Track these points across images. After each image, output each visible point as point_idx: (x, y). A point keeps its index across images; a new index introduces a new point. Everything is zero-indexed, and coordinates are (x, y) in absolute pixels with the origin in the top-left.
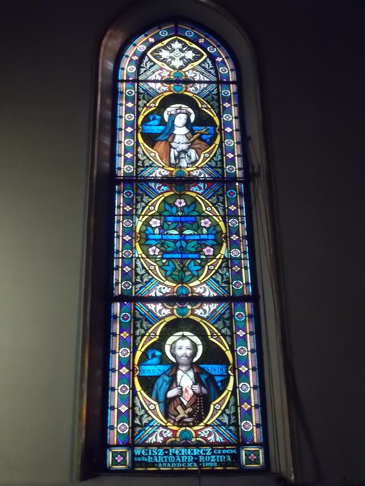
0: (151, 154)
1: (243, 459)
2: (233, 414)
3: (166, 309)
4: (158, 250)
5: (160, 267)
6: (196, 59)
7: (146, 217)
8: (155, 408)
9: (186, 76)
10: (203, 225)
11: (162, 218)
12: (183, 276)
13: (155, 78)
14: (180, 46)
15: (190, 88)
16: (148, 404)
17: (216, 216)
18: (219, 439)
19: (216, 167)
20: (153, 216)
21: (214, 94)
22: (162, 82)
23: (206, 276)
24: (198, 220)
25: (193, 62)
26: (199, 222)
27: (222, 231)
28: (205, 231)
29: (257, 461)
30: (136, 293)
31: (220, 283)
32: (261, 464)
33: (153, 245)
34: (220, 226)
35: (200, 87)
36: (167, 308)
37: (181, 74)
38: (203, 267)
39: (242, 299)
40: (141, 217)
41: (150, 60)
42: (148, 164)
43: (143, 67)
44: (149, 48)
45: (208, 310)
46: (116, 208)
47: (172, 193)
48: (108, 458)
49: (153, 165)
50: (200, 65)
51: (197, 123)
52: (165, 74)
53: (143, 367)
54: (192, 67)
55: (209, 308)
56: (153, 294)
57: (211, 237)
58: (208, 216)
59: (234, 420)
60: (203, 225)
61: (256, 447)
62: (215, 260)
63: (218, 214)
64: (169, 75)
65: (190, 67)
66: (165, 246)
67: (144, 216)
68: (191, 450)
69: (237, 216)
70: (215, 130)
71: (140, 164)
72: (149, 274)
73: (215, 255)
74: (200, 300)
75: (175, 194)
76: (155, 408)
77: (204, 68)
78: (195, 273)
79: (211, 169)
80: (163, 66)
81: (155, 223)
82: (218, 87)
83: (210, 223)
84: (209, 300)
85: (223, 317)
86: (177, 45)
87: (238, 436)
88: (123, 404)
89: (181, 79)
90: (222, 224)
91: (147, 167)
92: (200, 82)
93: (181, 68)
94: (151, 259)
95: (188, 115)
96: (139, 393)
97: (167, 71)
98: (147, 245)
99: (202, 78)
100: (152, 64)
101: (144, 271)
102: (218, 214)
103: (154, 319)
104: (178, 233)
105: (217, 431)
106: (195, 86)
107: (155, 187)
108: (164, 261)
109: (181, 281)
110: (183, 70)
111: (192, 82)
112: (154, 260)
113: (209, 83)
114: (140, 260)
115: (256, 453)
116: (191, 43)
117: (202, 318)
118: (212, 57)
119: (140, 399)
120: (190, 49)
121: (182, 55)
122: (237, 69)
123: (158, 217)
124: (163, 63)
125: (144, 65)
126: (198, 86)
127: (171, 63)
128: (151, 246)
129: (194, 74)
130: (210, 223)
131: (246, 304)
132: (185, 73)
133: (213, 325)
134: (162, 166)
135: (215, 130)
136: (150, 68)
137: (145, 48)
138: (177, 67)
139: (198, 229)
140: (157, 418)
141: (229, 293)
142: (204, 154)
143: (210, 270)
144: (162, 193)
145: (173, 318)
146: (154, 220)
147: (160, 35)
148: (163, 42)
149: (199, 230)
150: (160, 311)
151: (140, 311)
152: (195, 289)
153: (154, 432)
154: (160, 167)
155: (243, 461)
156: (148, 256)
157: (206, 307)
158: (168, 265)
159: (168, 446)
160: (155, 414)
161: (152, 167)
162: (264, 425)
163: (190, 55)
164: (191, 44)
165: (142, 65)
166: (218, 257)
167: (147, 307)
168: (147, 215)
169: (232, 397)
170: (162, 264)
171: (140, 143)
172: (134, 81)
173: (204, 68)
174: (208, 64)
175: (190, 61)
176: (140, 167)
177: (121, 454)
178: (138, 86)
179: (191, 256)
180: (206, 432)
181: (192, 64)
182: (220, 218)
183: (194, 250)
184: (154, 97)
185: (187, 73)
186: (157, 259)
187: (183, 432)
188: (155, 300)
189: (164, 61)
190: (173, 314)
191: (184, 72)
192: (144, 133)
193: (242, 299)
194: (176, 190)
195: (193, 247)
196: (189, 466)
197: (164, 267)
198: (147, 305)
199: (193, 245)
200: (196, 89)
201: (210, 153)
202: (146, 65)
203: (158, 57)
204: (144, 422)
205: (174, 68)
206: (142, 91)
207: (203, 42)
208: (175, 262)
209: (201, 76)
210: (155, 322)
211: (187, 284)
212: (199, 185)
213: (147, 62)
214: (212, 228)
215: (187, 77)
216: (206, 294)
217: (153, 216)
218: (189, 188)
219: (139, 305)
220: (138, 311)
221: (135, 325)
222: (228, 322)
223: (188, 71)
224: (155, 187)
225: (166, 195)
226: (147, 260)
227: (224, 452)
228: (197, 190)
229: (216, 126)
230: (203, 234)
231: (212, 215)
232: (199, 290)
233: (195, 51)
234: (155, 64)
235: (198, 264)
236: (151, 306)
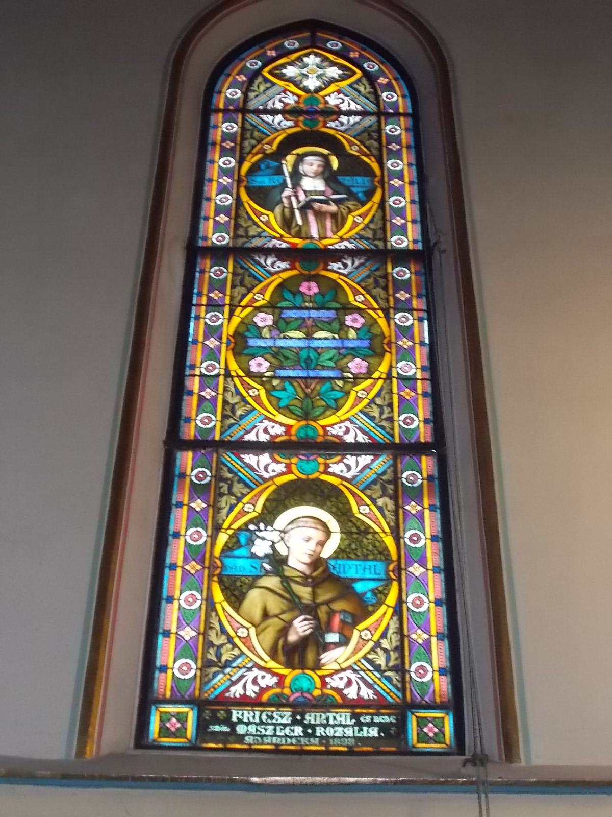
0: (261, 218)
1: (412, 734)
2: (396, 649)
3: (277, 464)
4: (267, 364)
5: (268, 392)
6: (342, 78)
7: (249, 310)
8: (249, 634)
9: (327, 102)
10: (348, 323)
11: (277, 311)
12: (310, 406)
13: (272, 106)
14: (318, 60)
15: (331, 122)
16: (234, 626)
17: (374, 309)
18: (367, 693)
19: (375, 239)
20: (259, 309)
21: (373, 131)
22: (283, 112)
23: (353, 407)
24: (341, 317)
25: (337, 81)
26: (342, 320)
27: (383, 334)
28: (352, 334)
29: (439, 737)
30: (222, 433)
31: (378, 420)
32: (448, 742)
33: (258, 355)
34: (380, 326)
35: (349, 121)
36: (278, 462)
37: (317, 100)
38: (348, 393)
39: (415, 449)
40: (239, 309)
41: (266, 80)
42: (255, 234)
43: (254, 91)
44: (264, 66)
45: (353, 465)
46: (195, 295)
47: (295, 272)
48: (427, 711)
49: (263, 234)
50: (351, 86)
51: (342, 170)
52: (291, 100)
53: (228, 561)
54: (337, 88)
55: (357, 462)
56: (251, 437)
57: (366, 343)
58: (358, 310)
59: (396, 659)
60: (348, 323)
61: (439, 711)
62: (369, 382)
63: (376, 306)
64: (297, 102)
65: (332, 88)
66: (280, 358)
67: (245, 307)
68: (267, 715)
69: (410, 310)
70: (373, 181)
71: (241, 232)
72: (235, 646)
73: (369, 374)
74: (339, 448)
75: (302, 274)
76: (249, 634)
77: (356, 90)
78: (332, 403)
79: (366, 242)
80: (287, 87)
81: (264, 320)
82: (379, 122)
83: (362, 320)
84: (357, 448)
85: (381, 479)
86: (312, 60)
87: (403, 690)
88: (188, 625)
89: (318, 109)
90: (382, 322)
91: (253, 237)
92: (349, 113)
93: (318, 90)
94: (253, 379)
95: (326, 158)
96: (218, 607)
97: (294, 94)
98: (247, 355)
99: (353, 106)
100: (268, 85)
101: (238, 397)
102: (376, 306)
103: (255, 482)
104: (305, 336)
105: (362, 679)
106: (340, 119)
107: (265, 262)
108: (276, 382)
109: (306, 416)
110: (322, 93)
111: (337, 113)
112: (257, 379)
113: (364, 114)
114: (233, 380)
115: (182, 718)
116: (336, 57)
117: (343, 478)
118: (370, 78)
119: (219, 617)
120: (333, 64)
121: (320, 71)
122: (413, 94)
123: (270, 310)
124: (287, 83)
125: (255, 87)
126: (344, 119)
127: (301, 83)
128: (253, 357)
129: (341, 101)
130: (362, 320)
131: (424, 458)
132: (324, 98)
133: (362, 491)
134: (278, 236)
135: (373, 181)
136: (264, 91)
137: (260, 63)
138: (312, 88)
139: (340, 330)
140: (253, 653)
141: (392, 436)
142: (354, 217)
143: (359, 400)
144: (277, 273)
145: (291, 477)
146: (261, 315)
147: (285, 47)
148: (289, 56)
149: (342, 333)
150: (266, 468)
151: (230, 465)
152: (329, 429)
153: (242, 676)
154: (275, 238)
155: (412, 739)
156: (249, 374)
157: (351, 460)
158: (284, 389)
159: (269, 704)
160: (247, 645)
161: (260, 237)
162: (454, 670)
163: (334, 72)
164: (335, 59)
165: (252, 88)
166: (376, 375)
167: (242, 460)
168: (251, 306)
169: (395, 618)
170: (272, 387)
171: (242, 202)
172: (237, 110)
173: (356, 90)
174: (364, 85)
175: (333, 81)
176: (242, 236)
177: (434, 722)
178: (244, 119)
179: (325, 374)
180: (341, 678)
181: (337, 84)
182: (380, 313)
183: (332, 364)
184: (262, 279)
185: (327, 98)
186: (264, 379)
187: (297, 679)
188: (257, 447)
189: (290, 80)
190: (289, 471)
191: (323, 97)
192: (250, 187)
193: (415, 449)
194: (304, 268)
195: (331, 359)
196: (303, 743)
197: (276, 393)
198: (242, 456)
199: (330, 356)
200: (342, 124)
201: (363, 216)
202: (258, 87)
203: (281, 77)
204: (224, 659)
205: (306, 90)
206: (250, 127)
207: (357, 56)
208: (295, 384)
209: (352, 103)
210: (256, 485)
211: (315, 421)
212: (344, 261)
213: (261, 83)
214: (365, 329)
215: (327, 105)
216: (349, 439)
217: (259, 309)
218: (326, 265)
219: (229, 458)
220: (226, 466)
221: (218, 488)
222: (390, 488)
223: (329, 95)
224: (265, 262)
225: (285, 275)
226: (247, 379)
227: (377, 719)
228: (339, 268)
229: (374, 175)
230: (348, 338)
231: (366, 307)
232: (337, 431)
233: (341, 67)
234: (274, 84)
235: (338, 388)
236: (250, 459)
